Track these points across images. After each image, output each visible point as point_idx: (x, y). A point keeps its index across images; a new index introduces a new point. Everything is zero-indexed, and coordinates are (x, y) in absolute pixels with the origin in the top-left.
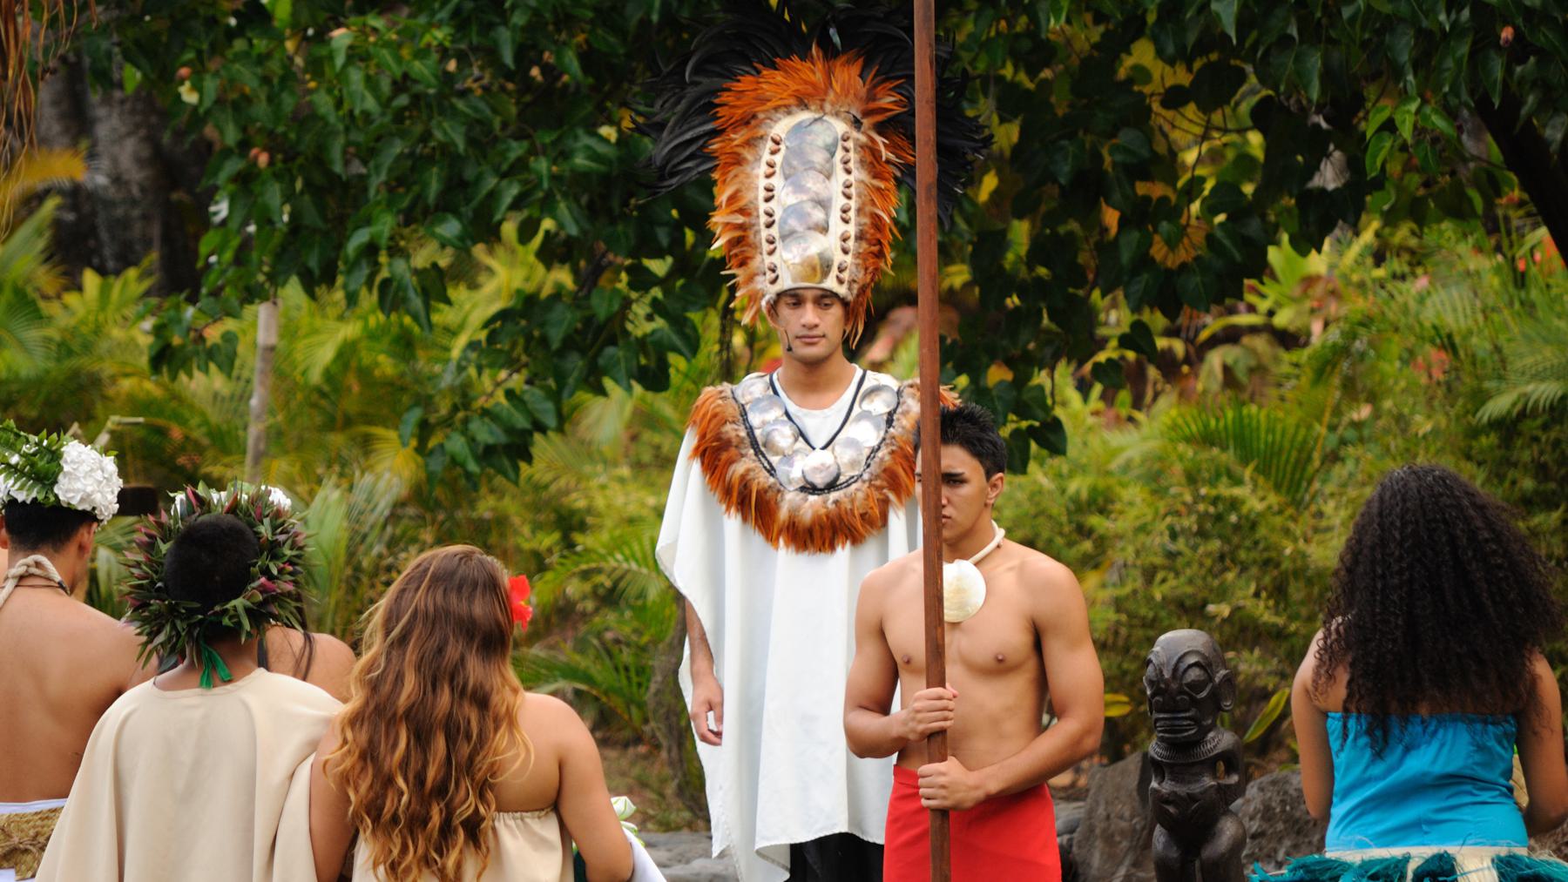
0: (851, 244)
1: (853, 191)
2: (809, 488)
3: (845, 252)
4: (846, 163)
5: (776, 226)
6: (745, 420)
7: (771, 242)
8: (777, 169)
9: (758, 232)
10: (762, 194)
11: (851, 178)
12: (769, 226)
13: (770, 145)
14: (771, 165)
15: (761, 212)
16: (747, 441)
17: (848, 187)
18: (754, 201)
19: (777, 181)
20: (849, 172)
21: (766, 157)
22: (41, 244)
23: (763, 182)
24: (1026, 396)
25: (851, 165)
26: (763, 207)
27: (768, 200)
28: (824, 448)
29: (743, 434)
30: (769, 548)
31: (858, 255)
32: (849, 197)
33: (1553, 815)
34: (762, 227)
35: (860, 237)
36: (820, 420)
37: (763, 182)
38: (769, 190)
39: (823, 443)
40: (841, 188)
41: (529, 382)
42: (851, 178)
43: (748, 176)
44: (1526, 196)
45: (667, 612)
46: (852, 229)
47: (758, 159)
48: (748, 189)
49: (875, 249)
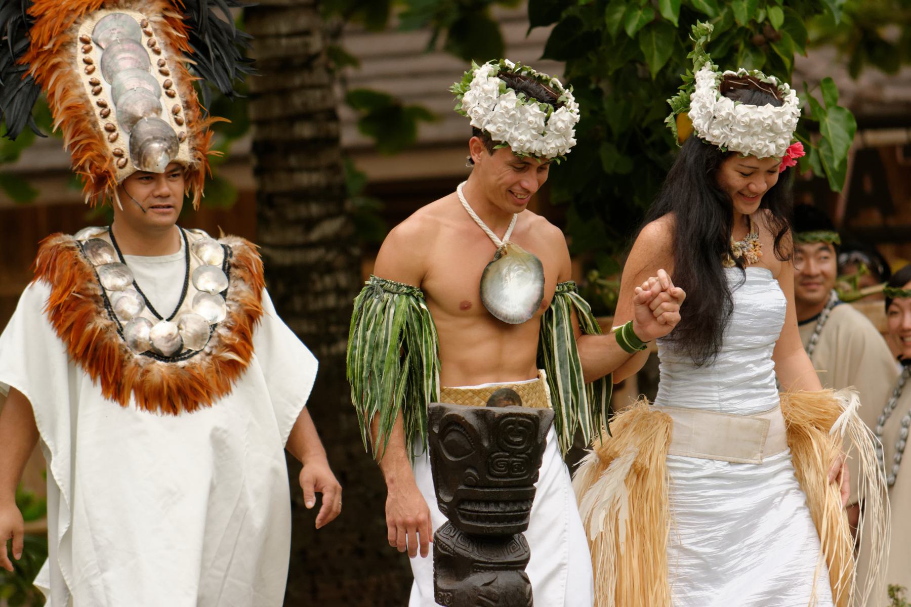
0: (182, 115)
1: (166, 68)
2: (154, 353)
3: (180, 123)
4: (153, 45)
9: (95, 124)
10: (89, 89)
12: (105, 116)
13: (80, 45)
17: (163, 65)
20: (158, 52)
21: (80, 56)
22: (139, 408)
26: (94, 100)
27: (97, 93)
28: (169, 320)
30: (114, 406)
32: (166, 74)
35: (188, 106)
37: (85, 79)
39: (167, 317)
40: (157, 68)
41: (183, 21)
43: (70, 73)
44: (36, 296)
46: (178, 101)
47: (73, 57)
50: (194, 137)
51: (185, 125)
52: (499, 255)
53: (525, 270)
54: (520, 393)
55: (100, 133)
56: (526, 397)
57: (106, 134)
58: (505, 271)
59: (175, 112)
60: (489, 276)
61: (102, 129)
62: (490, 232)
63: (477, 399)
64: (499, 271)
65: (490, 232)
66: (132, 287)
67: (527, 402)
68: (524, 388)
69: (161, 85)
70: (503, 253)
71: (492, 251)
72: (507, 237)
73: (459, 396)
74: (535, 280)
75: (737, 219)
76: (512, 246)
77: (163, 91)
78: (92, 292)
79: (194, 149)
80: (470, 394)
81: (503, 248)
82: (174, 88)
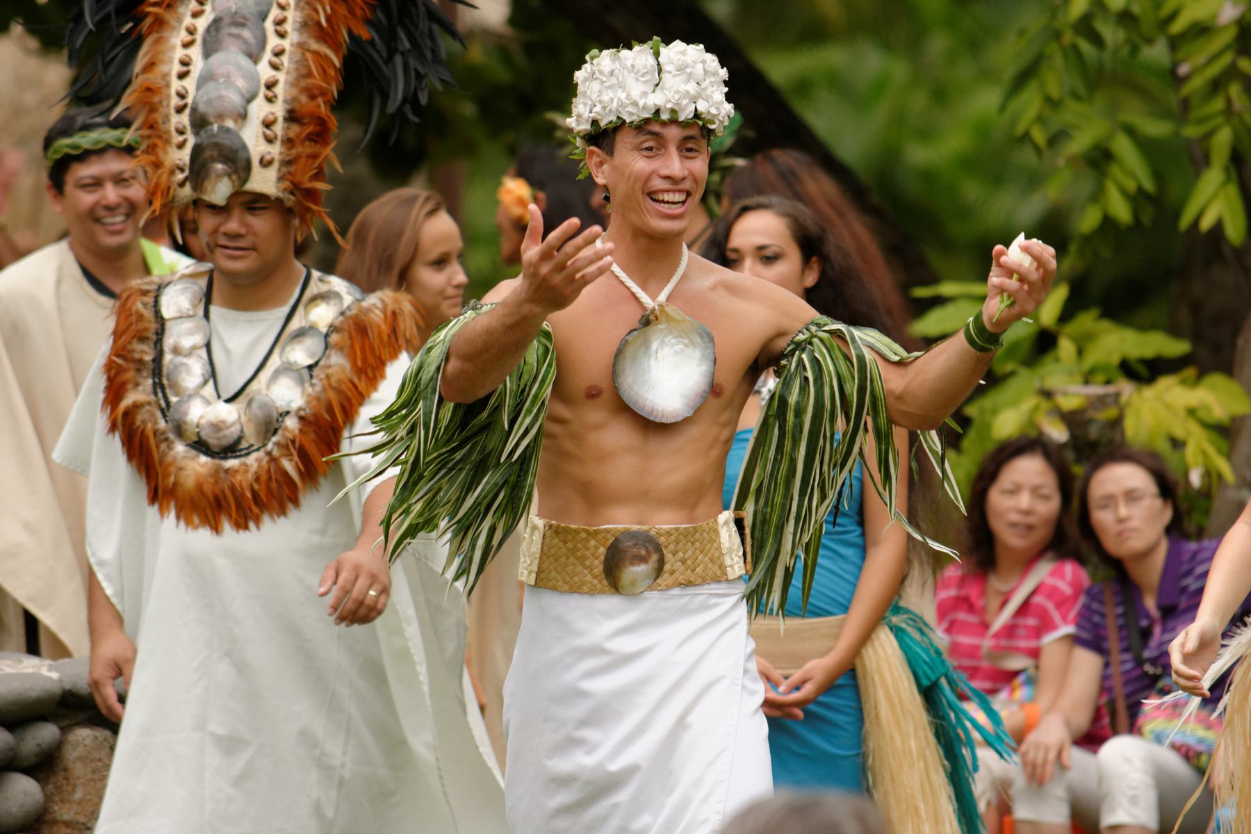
0: (279, 129)
5: (187, 111)
6: (159, 342)
7: (181, 132)
8: (199, 37)
9: (167, 118)
10: (177, 68)
11: (286, 44)
14: (191, 31)
15: (173, 92)
16: (151, 366)
18: (166, 76)
19: (195, 53)
21: (188, 21)
23: (179, 53)
24: (428, 299)
25: (288, 27)
29: (148, 358)
31: (289, 142)
33: (902, 604)
34: (173, 111)
35: (292, 116)
36: (242, 337)
38: (185, 63)
42: (286, 44)
45: (1026, 262)
46: (279, 110)
48: (163, 62)
49: (147, 108)
50: (287, 163)
51: (278, 143)
52: (647, 321)
53: (686, 345)
54: (662, 540)
55: (168, 132)
56: (672, 547)
57: (174, 134)
58: (655, 346)
59: (268, 124)
60: (629, 352)
61: (173, 129)
62: (636, 289)
63: (593, 543)
64: (646, 345)
65: (636, 289)
66: (203, 353)
67: (674, 554)
68: (669, 533)
69: (263, 82)
70: (652, 317)
71: (637, 314)
72: (662, 297)
73: (570, 537)
74: (701, 360)
75: (402, 342)
76: (667, 309)
77: (263, 90)
78: (137, 356)
79: (281, 179)
80: (583, 535)
81: (653, 311)
82: (279, 90)
